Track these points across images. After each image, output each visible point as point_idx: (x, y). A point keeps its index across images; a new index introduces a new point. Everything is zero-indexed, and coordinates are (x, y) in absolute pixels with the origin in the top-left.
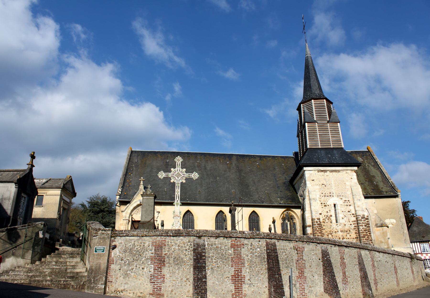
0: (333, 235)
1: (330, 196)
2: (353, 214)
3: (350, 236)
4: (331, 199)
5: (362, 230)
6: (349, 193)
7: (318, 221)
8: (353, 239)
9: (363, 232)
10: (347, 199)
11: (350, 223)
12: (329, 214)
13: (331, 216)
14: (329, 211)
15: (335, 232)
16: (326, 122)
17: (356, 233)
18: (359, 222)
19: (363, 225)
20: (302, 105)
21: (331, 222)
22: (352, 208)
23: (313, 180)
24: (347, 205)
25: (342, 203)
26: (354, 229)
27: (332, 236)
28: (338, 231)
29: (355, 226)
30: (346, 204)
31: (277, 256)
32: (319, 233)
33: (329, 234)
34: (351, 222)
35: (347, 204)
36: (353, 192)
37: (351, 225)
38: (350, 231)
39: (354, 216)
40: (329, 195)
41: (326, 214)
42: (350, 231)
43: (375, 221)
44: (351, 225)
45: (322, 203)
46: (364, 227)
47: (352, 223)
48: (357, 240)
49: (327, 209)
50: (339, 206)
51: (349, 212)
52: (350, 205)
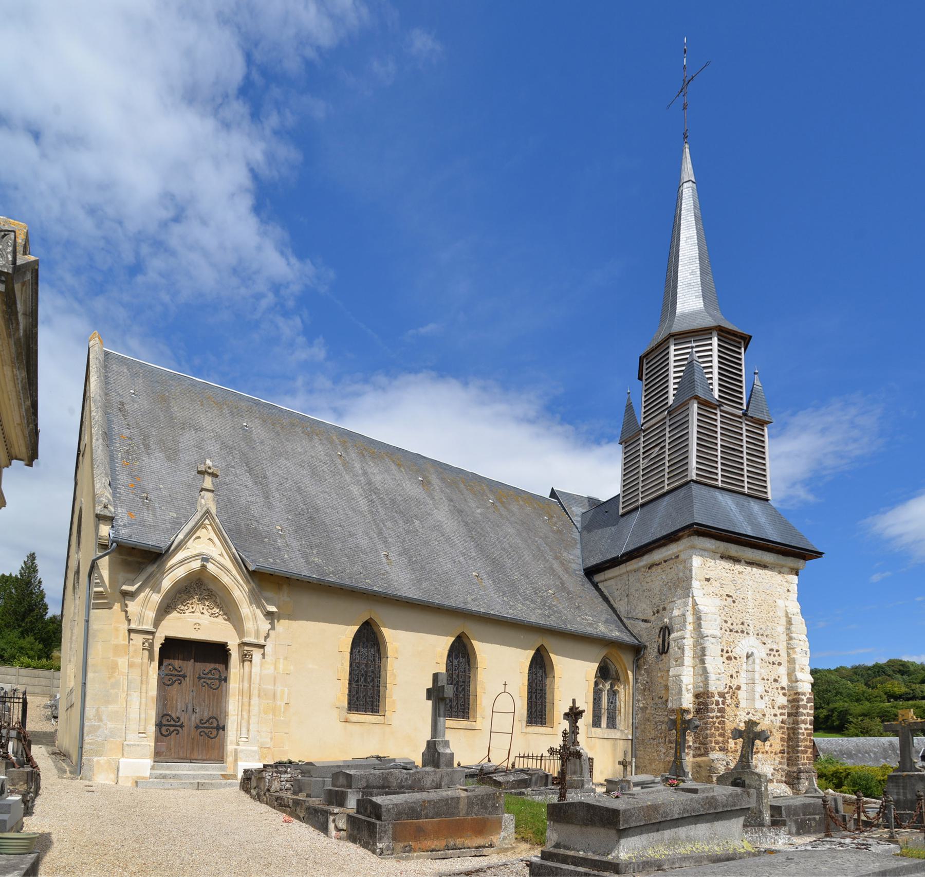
1: (742, 632)
2: (783, 688)
6: (781, 629)
7: (721, 700)
8: (776, 754)
10: (775, 647)
11: (773, 712)
12: (735, 683)
14: (735, 676)
17: (782, 739)
18: (801, 710)
22: (782, 671)
23: (708, 580)
25: (764, 656)
26: (781, 728)
29: (782, 722)
30: (772, 659)
31: (516, 827)
32: (720, 735)
34: (776, 708)
39: (784, 695)
40: (740, 627)
44: (775, 715)
47: (778, 712)
48: (782, 758)
49: (731, 668)
51: (775, 680)
52: (780, 664)
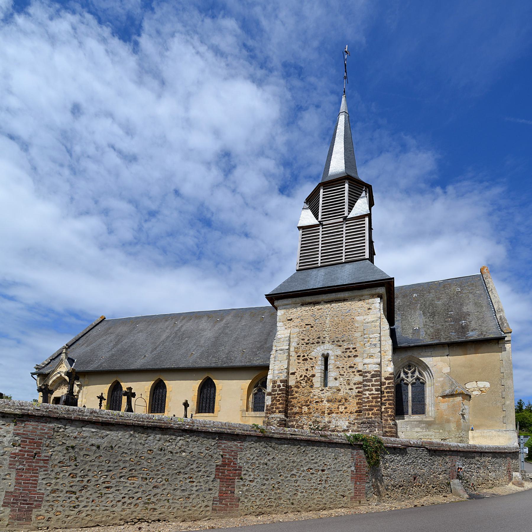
0: (311, 406)
1: (318, 343)
3: (346, 408)
4: (318, 348)
5: (368, 398)
9: (369, 402)
13: (313, 376)
15: (316, 402)
16: (341, 220)
19: (374, 388)
20: (322, 191)
21: (312, 386)
23: (291, 320)
24: (349, 357)
26: (357, 396)
27: (309, 409)
28: (322, 401)
30: (348, 354)
33: (303, 406)
34: (352, 384)
35: (350, 354)
36: (398, 331)
37: (351, 389)
38: (346, 400)
41: (304, 374)
42: (346, 400)
43: (442, 387)
45: (298, 356)
46: (374, 392)
47: (354, 387)
50: (332, 358)
51: (350, 367)
